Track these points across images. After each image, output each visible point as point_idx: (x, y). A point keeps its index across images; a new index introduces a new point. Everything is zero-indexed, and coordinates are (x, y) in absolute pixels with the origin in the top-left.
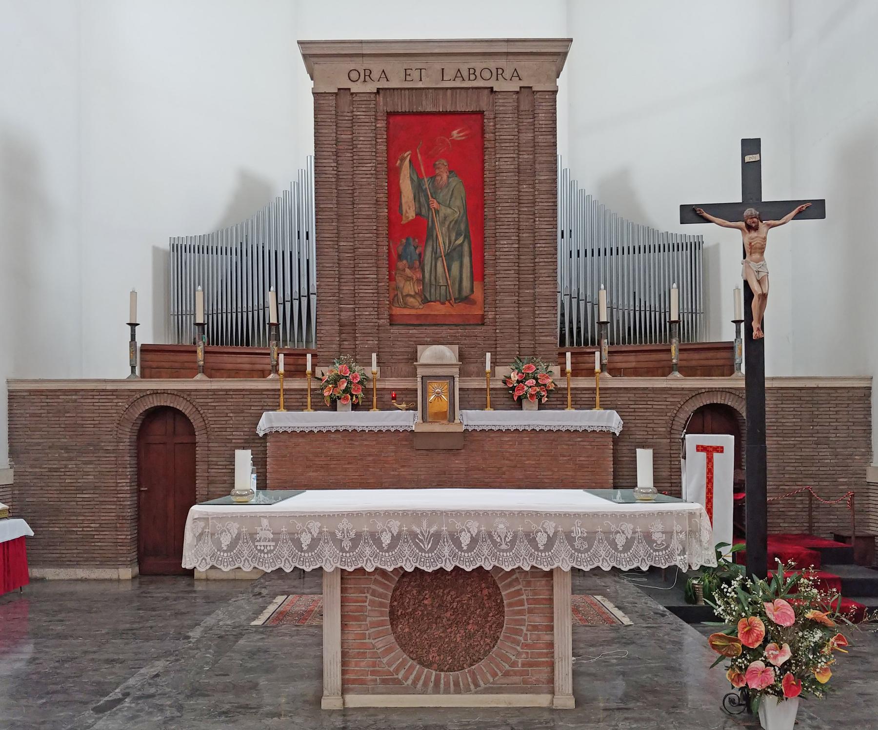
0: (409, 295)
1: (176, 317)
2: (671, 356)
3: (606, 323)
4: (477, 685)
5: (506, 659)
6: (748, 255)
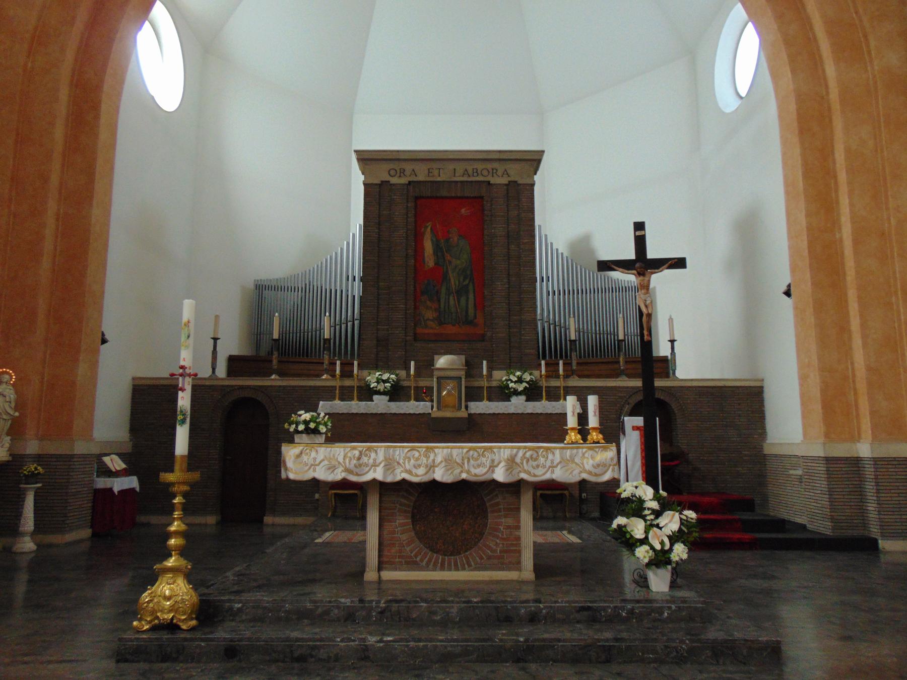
0: (428, 319)
1: (256, 336)
2: (620, 365)
3: (575, 341)
4: (470, 565)
5: (489, 548)
6: (639, 290)
